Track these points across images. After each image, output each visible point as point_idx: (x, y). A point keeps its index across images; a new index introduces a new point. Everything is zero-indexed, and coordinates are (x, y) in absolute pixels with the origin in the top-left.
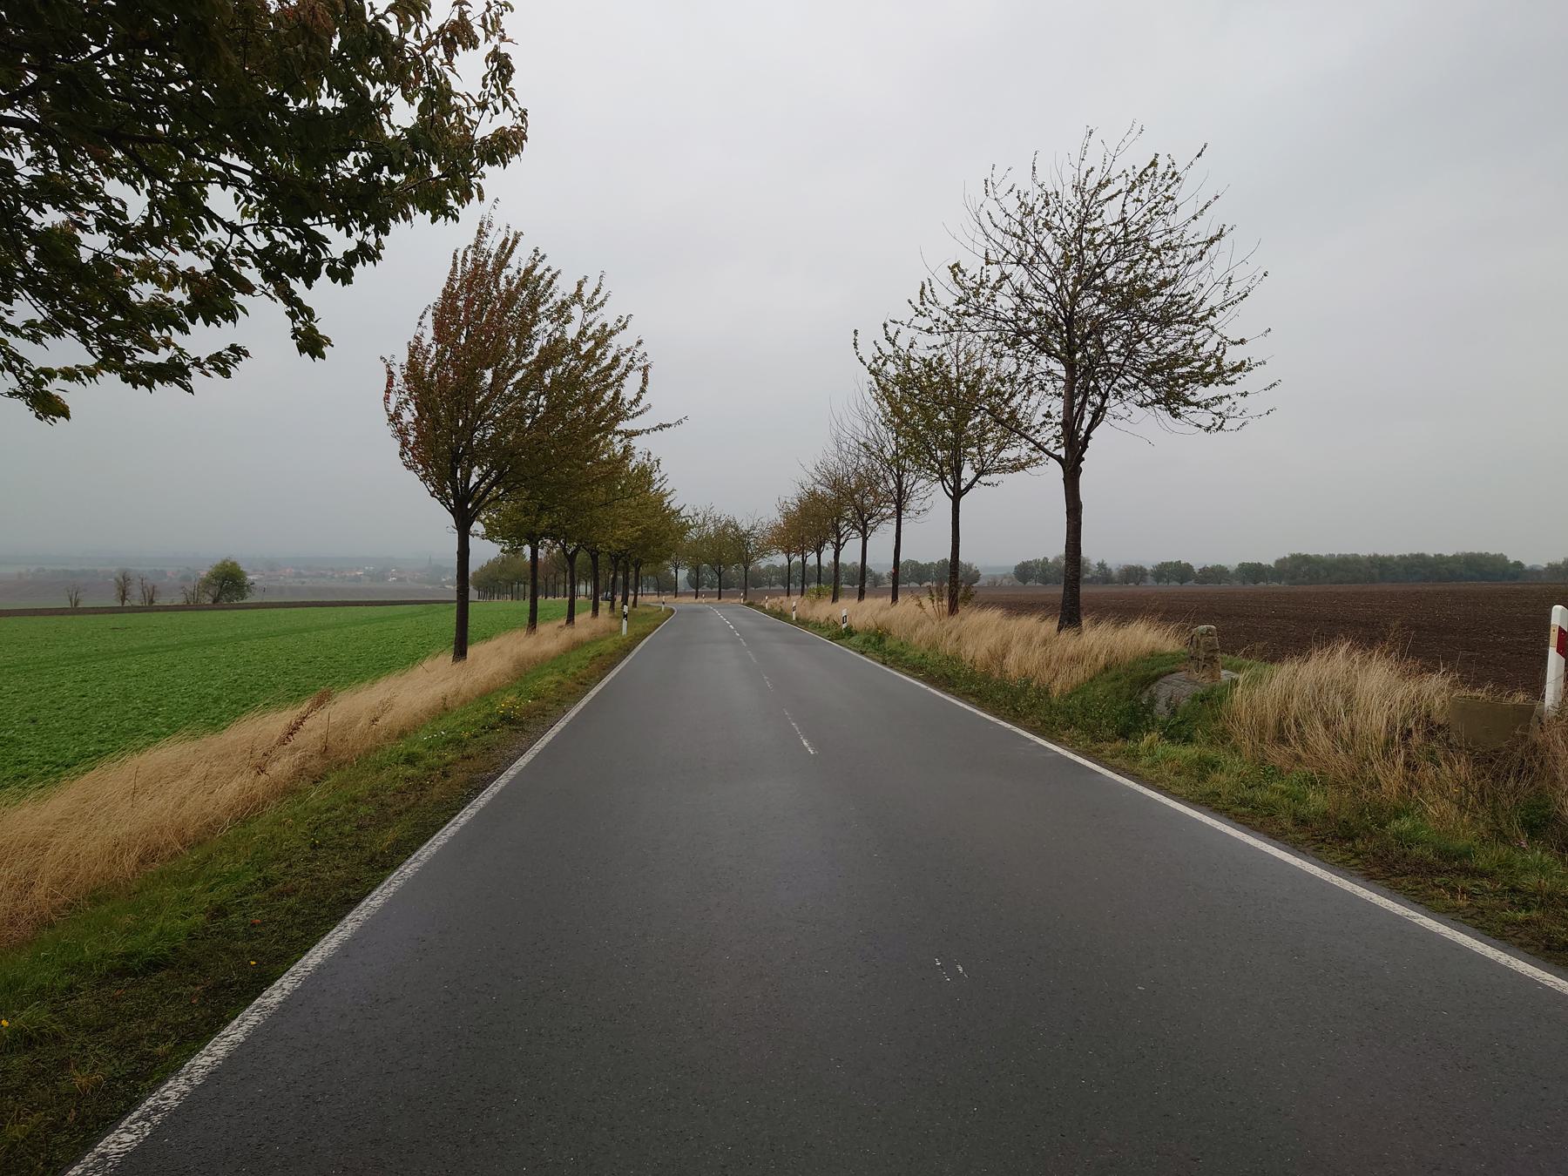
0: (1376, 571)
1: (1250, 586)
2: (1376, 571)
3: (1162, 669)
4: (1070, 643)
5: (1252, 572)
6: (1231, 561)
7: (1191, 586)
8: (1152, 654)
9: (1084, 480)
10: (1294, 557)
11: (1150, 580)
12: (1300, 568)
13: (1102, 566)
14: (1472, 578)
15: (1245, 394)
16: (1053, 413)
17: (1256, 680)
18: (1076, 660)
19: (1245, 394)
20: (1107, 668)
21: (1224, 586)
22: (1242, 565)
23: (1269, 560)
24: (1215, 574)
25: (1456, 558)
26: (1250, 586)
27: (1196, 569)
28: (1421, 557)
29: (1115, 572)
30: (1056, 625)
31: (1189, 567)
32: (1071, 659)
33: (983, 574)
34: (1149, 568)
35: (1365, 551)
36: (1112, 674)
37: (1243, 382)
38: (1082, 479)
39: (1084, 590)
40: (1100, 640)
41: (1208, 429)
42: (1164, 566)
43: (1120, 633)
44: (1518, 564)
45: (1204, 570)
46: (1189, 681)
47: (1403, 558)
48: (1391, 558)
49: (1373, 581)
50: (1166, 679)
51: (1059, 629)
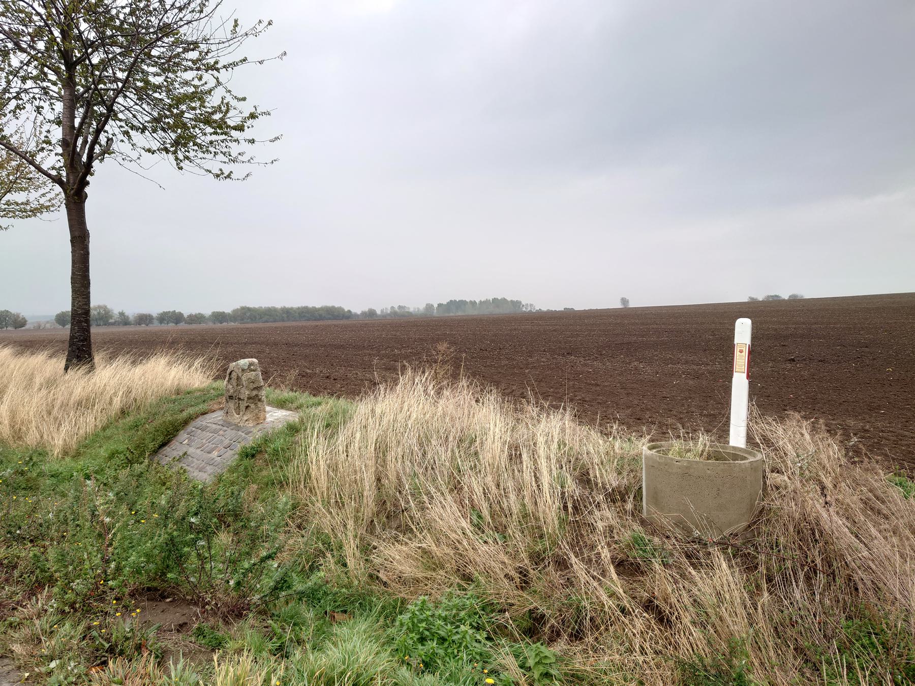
0: (285, 315)
1: (218, 325)
2: (285, 315)
3: (191, 410)
4: (78, 383)
5: (219, 317)
6: (207, 312)
7: (182, 326)
8: (178, 392)
9: (90, 206)
10: (243, 308)
11: (156, 322)
12: (245, 314)
13: (122, 314)
14: (330, 319)
15: (252, 141)
16: (54, 141)
17: (331, 426)
18: (84, 404)
19: (252, 141)
20: (123, 413)
21: (203, 326)
22: (214, 313)
23: (228, 309)
24: (197, 319)
25: (322, 309)
26: (218, 325)
27: (186, 316)
28: (306, 308)
29: (131, 318)
30: (63, 363)
31: (181, 314)
32: (79, 404)
33: (29, 321)
34: (155, 315)
35: (279, 305)
36: (129, 420)
37: (254, 130)
38: (88, 205)
39: (94, 330)
40: (114, 379)
41: (218, 176)
42: (165, 313)
43: (139, 370)
44: (349, 311)
45: (190, 316)
46: (227, 424)
47: (299, 308)
48: (292, 308)
49: (283, 321)
50: (199, 422)
51: (66, 369)
